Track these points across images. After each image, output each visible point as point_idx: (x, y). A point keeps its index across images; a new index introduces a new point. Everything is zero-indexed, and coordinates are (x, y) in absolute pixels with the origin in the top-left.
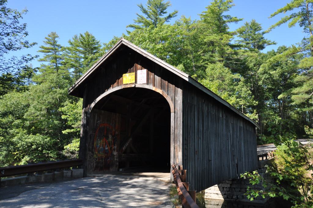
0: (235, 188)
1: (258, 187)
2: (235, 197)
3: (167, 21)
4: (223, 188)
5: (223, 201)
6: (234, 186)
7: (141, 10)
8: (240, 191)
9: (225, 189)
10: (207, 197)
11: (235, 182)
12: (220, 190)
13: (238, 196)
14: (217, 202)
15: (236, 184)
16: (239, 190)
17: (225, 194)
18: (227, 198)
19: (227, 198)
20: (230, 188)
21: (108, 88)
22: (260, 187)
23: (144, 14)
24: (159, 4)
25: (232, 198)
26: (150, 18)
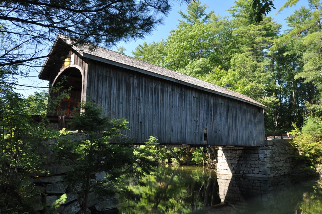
0: (241, 164)
1: (262, 162)
2: (241, 172)
3: (206, 22)
4: (232, 164)
5: (232, 176)
6: (241, 162)
7: (181, 16)
8: (246, 167)
9: (233, 165)
10: (219, 173)
11: (242, 159)
12: (229, 166)
13: (244, 171)
14: (227, 177)
15: (243, 160)
16: (245, 165)
17: (233, 170)
18: (235, 173)
19: (235, 173)
20: (238, 164)
21: (59, 71)
22: (263, 162)
23: (184, 19)
24: (197, 8)
25: (239, 173)
26: (190, 21)
